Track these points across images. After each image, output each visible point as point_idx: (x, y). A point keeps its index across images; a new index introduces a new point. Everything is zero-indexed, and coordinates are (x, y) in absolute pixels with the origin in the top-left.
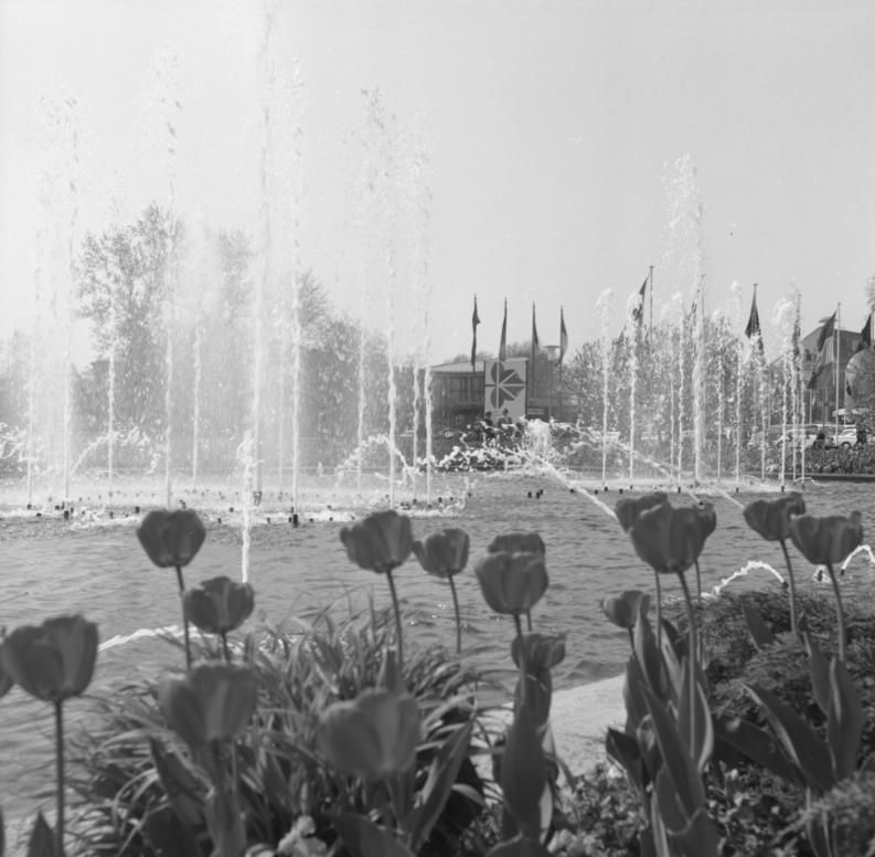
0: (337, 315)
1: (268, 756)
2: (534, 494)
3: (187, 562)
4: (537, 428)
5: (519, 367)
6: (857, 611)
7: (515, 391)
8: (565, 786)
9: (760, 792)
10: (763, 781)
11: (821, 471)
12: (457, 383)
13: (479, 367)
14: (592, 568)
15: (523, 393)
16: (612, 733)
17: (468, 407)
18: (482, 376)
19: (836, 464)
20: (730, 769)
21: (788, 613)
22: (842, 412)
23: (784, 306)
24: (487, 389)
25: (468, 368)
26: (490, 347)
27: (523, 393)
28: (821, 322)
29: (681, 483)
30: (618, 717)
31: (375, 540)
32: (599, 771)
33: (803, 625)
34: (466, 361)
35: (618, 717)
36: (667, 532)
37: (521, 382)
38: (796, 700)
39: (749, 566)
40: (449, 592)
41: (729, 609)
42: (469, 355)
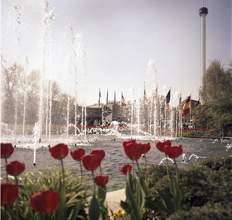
0: (63, 92)
1: (29, 209)
2: (113, 140)
3: (8, 157)
4: (115, 123)
5: (111, 107)
6: (184, 170)
7: (110, 113)
8: (111, 216)
9: (161, 216)
10: (162, 213)
11: (186, 135)
12: (95, 110)
13: (101, 107)
14: (114, 160)
15: (112, 114)
16: (122, 202)
17: (94, 117)
18: (101, 109)
19: (190, 133)
20: (152, 210)
21: (166, 170)
22: (192, 120)
23: (177, 93)
24: (102, 112)
25: (97, 107)
26: (104, 102)
27: (112, 114)
28: (187, 97)
29: (140, 138)
30: (124, 199)
31: (59, 151)
32: (120, 211)
33: (170, 173)
34: (97, 105)
35: (124, 199)
36: (134, 149)
37: (112, 111)
38: (166, 193)
39: (157, 158)
40: (60, 163)
41: (153, 170)
42: (98, 103)
